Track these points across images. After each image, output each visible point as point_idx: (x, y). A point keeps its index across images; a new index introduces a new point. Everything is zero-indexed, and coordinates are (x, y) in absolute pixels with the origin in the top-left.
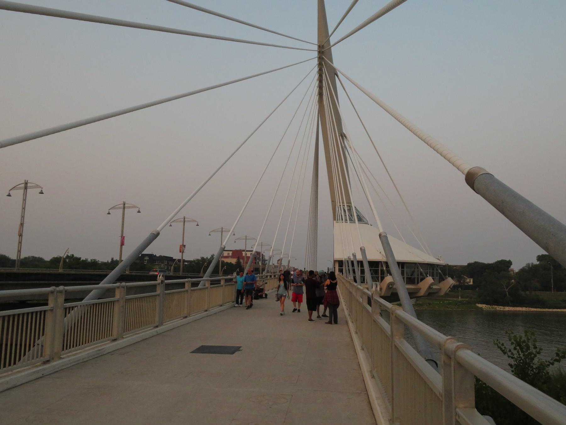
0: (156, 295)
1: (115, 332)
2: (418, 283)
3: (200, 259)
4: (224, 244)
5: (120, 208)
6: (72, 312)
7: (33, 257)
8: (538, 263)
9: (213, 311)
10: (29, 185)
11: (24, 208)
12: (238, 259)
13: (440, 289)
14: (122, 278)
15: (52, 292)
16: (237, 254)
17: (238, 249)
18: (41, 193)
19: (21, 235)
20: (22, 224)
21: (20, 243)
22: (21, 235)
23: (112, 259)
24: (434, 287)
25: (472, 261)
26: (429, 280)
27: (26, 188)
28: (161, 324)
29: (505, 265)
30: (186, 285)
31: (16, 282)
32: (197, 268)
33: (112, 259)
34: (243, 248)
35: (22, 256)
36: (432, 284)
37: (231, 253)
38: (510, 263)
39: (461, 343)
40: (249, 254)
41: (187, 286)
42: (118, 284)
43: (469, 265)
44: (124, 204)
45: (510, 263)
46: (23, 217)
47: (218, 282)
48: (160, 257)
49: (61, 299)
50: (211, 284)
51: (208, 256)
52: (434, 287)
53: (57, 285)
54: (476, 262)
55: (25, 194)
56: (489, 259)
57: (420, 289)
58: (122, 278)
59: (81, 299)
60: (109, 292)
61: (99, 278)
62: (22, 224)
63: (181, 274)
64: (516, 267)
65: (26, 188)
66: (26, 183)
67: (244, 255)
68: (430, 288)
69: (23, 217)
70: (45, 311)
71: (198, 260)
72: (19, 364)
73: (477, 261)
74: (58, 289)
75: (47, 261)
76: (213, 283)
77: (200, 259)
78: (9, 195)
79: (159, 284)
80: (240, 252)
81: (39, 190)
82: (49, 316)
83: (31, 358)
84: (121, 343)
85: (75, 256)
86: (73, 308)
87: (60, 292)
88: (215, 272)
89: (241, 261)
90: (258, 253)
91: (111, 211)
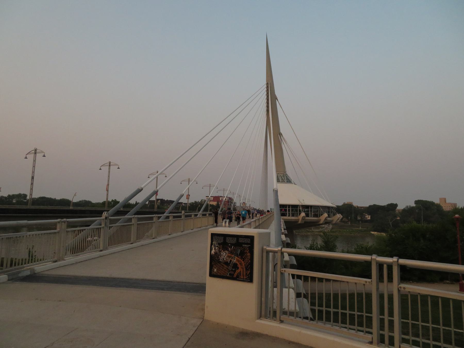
0: (55, 233)
1: (132, 240)
3: (413, 205)
4: (158, 188)
5: (107, 165)
6: (82, 233)
7: (85, 200)
8: (414, 205)
9: (195, 230)
10: (37, 151)
12: (218, 202)
13: (333, 220)
14: (138, 213)
15: (59, 222)
16: (216, 198)
17: (217, 196)
18: (44, 156)
19: (107, 190)
21: (107, 194)
22: (107, 190)
23: (136, 202)
25: (372, 204)
27: (35, 153)
28: (184, 231)
29: (393, 206)
30: (182, 216)
31: (35, 215)
32: (195, 207)
33: (136, 202)
34: (220, 195)
35: (110, 200)
36: (327, 217)
37: (212, 198)
38: (396, 205)
41: (193, 216)
42: (133, 216)
43: (370, 206)
44: (110, 163)
45: (396, 205)
46: (33, 172)
47: (205, 215)
48: (167, 200)
49: (64, 226)
50: (185, 217)
51: (199, 200)
53: (62, 217)
54: (374, 205)
55: (109, 169)
56: (383, 203)
58: (138, 213)
59: (89, 226)
60: (130, 220)
61: (100, 213)
63: (155, 210)
64: (401, 207)
65: (35, 153)
66: (36, 150)
68: (326, 219)
69: (33, 172)
70: (100, 228)
71: (192, 203)
72: (84, 252)
74: (62, 220)
76: (203, 215)
77: (413, 205)
78: (100, 169)
79: (103, 219)
80: (218, 197)
81: (43, 154)
82: (102, 230)
83: (9, 265)
84: (135, 245)
85: (355, 204)
86: (84, 230)
87: (64, 222)
88: (206, 210)
89: (220, 203)
91: (102, 168)
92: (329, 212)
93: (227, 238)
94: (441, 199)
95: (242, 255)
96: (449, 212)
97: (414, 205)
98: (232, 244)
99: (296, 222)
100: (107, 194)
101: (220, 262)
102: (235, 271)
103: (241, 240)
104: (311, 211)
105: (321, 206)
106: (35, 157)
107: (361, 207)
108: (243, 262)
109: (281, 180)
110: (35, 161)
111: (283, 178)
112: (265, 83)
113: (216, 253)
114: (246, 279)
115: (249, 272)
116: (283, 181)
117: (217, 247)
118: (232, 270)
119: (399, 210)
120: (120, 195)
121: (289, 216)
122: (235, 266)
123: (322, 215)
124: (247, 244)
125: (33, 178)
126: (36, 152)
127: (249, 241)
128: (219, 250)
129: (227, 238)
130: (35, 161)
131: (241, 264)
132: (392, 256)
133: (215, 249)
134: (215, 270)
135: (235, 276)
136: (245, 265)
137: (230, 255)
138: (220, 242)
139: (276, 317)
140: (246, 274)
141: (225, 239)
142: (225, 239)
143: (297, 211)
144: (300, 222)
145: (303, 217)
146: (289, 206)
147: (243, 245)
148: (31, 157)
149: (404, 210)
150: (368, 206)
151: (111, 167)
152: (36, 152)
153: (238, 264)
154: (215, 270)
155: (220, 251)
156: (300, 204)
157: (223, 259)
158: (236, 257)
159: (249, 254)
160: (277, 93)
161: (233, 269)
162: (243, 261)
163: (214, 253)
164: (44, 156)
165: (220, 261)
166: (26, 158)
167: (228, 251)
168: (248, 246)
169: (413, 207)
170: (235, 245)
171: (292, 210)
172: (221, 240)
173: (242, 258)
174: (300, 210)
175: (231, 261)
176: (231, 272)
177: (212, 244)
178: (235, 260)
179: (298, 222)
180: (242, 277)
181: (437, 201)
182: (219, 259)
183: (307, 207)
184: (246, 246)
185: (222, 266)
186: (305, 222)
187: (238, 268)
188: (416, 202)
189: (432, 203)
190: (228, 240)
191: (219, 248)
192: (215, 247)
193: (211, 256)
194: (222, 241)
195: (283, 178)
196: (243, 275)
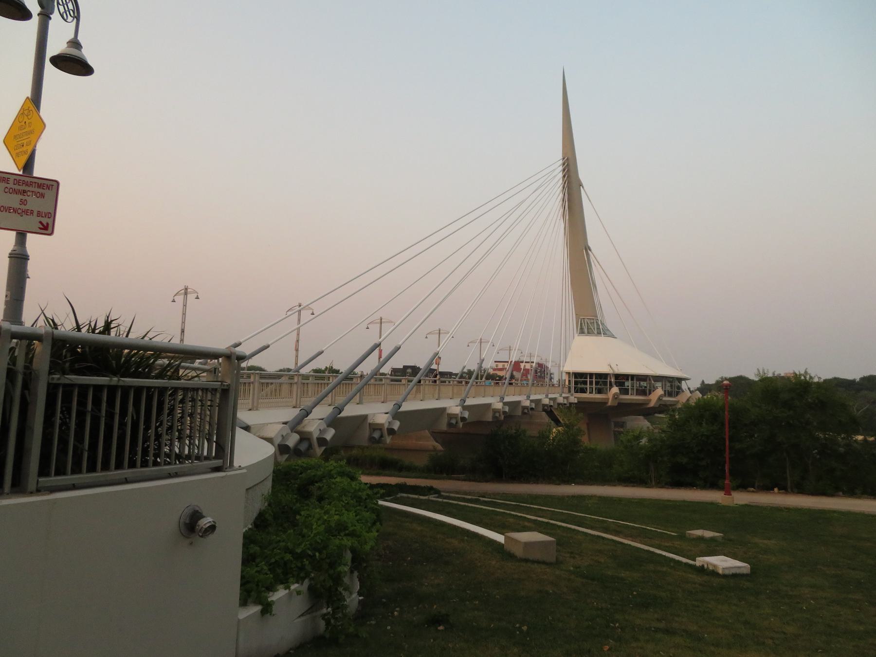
2: (650, 393)
11: (184, 314)
13: (678, 402)
18: (197, 298)
19: (297, 350)
20: (298, 341)
21: (297, 356)
22: (297, 350)
24: (665, 399)
26: (615, 390)
36: (661, 396)
39: (381, 502)
40: (528, 366)
46: (183, 322)
52: (665, 399)
57: (650, 400)
62: (298, 341)
65: (186, 294)
66: (186, 289)
67: (522, 367)
68: (659, 399)
69: (183, 322)
73: (837, 376)
75: (712, 385)
78: (174, 301)
81: (195, 295)
90: (540, 365)
99: (604, 403)
100: (297, 356)
104: (591, 383)
105: (653, 376)
106: (185, 300)
109: (586, 331)
110: (185, 305)
111: (589, 323)
112: (560, 156)
116: (590, 332)
120: (489, 365)
121: (591, 393)
125: (183, 331)
126: (186, 291)
130: (185, 305)
139: (49, 384)
143: (605, 383)
144: (609, 404)
145: (615, 394)
146: (591, 375)
148: (180, 299)
151: (75, 325)
152: (186, 291)
156: (611, 372)
160: (583, 175)
164: (197, 298)
166: (174, 301)
171: (597, 383)
174: (610, 382)
179: (607, 403)
183: (621, 379)
186: (619, 404)
195: (589, 323)
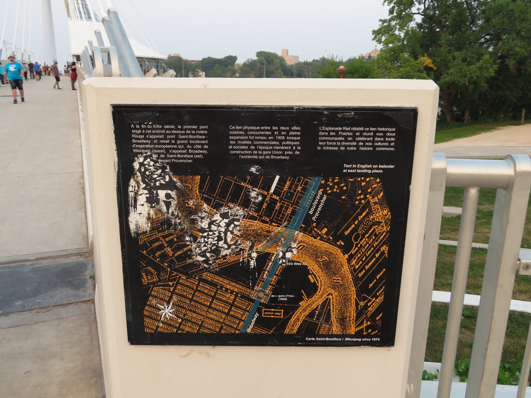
3: (255, 58)
8: (256, 58)
38: (234, 59)
43: (204, 60)
45: (234, 59)
54: (209, 58)
77: (255, 58)
85: (184, 57)
92: (157, 67)
93: (236, 132)
94: (283, 50)
95: (337, 220)
96: (292, 66)
97: (256, 58)
98: (270, 166)
101: (192, 270)
102: (291, 308)
103: (329, 140)
105: (146, 58)
107: (192, 61)
108: (343, 258)
113: (160, 224)
114: (359, 334)
115: (375, 303)
117: (170, 185)
118: (273, 303)
119: (238, 65)
122: (296, 281)
123: (148, 72)
124: (374, 157)
127: (385, 140)
128: (182, 206)
129: (236, 132)
131: (329, 267)
132: (256, 126)
133: (152, 200)
134: (167, 311)
135: (293, 326)
136: (354, 272)
137: (256, 225)
138: (183, 156)
140: (360, 313)
141: (218, 140)
142: (218, 140)
147: (348, 168)
149: (245, 64)
150: (201, 59)
153: (313, 266)
154: (167, 311)
155: (189, 213)
157: (216, 251)
158: (300, 235)
159: (382, 214)
161: (282, 298)
162: (345, 250)
163: (145, 226)
165: (195, 265)
167: (246, 203)
168: (379, 169)
169: (254, 61)
170: (293, 168)
172: (196, 142)
173: (335, 237)
175: (263, 258)
176: (269, 314)
177: (125, 173)
178: (293, 248)
180: (336, 329)
181: (280, 54)
182: (188, 255)
184: (364, 168)
185: (206, 288)
187: (312, 289)
188: (259, 54)
189: (275, 56)
190: (241, 141)
191: (183, 195)
192: (151, 189)
193: (129, 241)
194: (199, 153)
196: (342, 320)
